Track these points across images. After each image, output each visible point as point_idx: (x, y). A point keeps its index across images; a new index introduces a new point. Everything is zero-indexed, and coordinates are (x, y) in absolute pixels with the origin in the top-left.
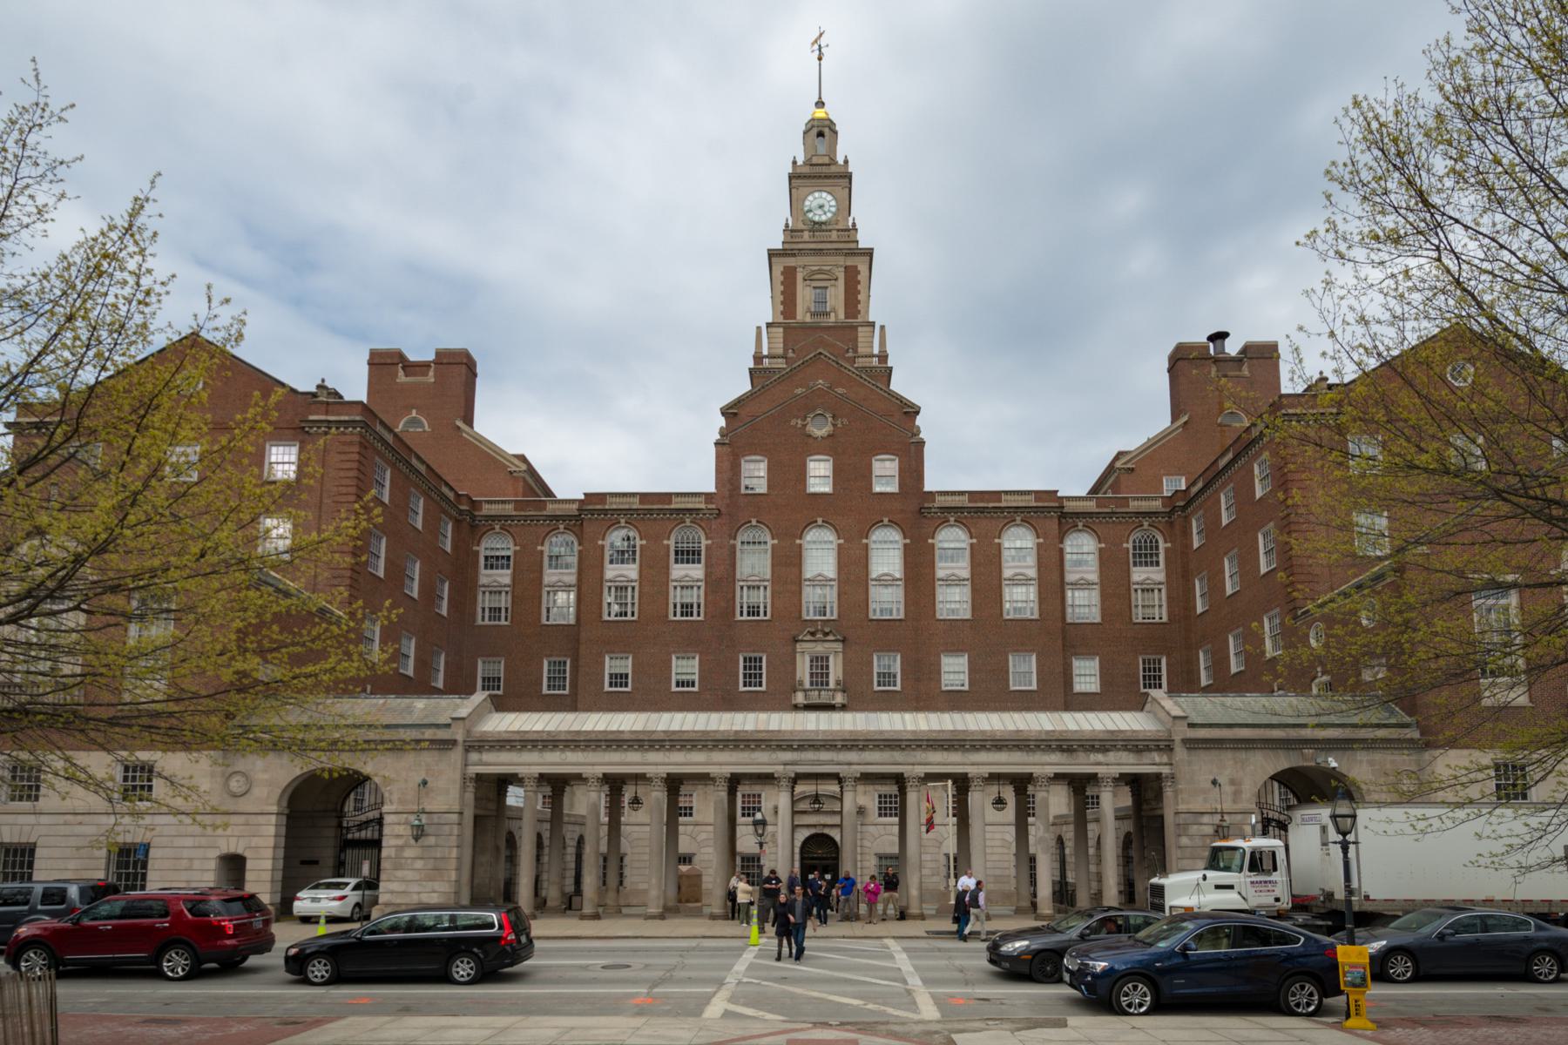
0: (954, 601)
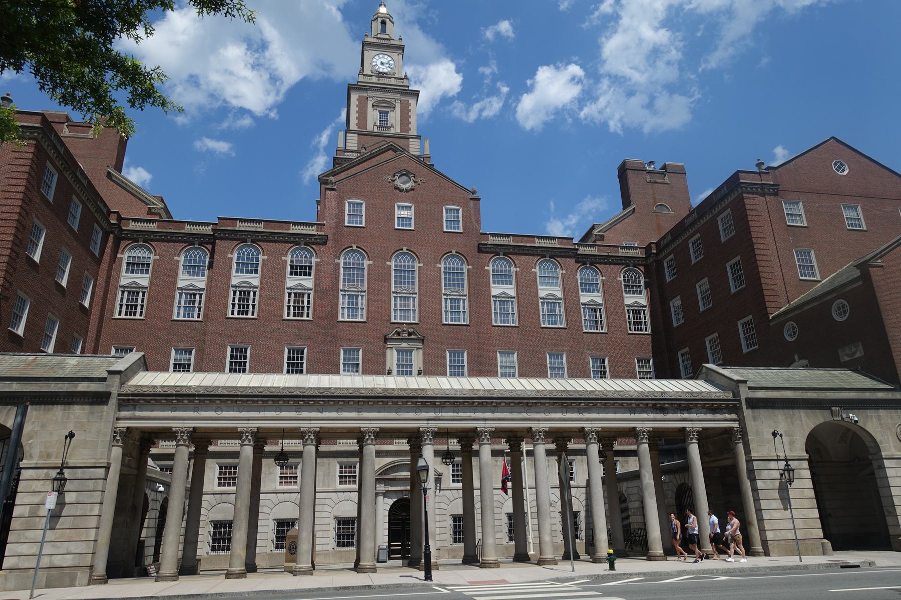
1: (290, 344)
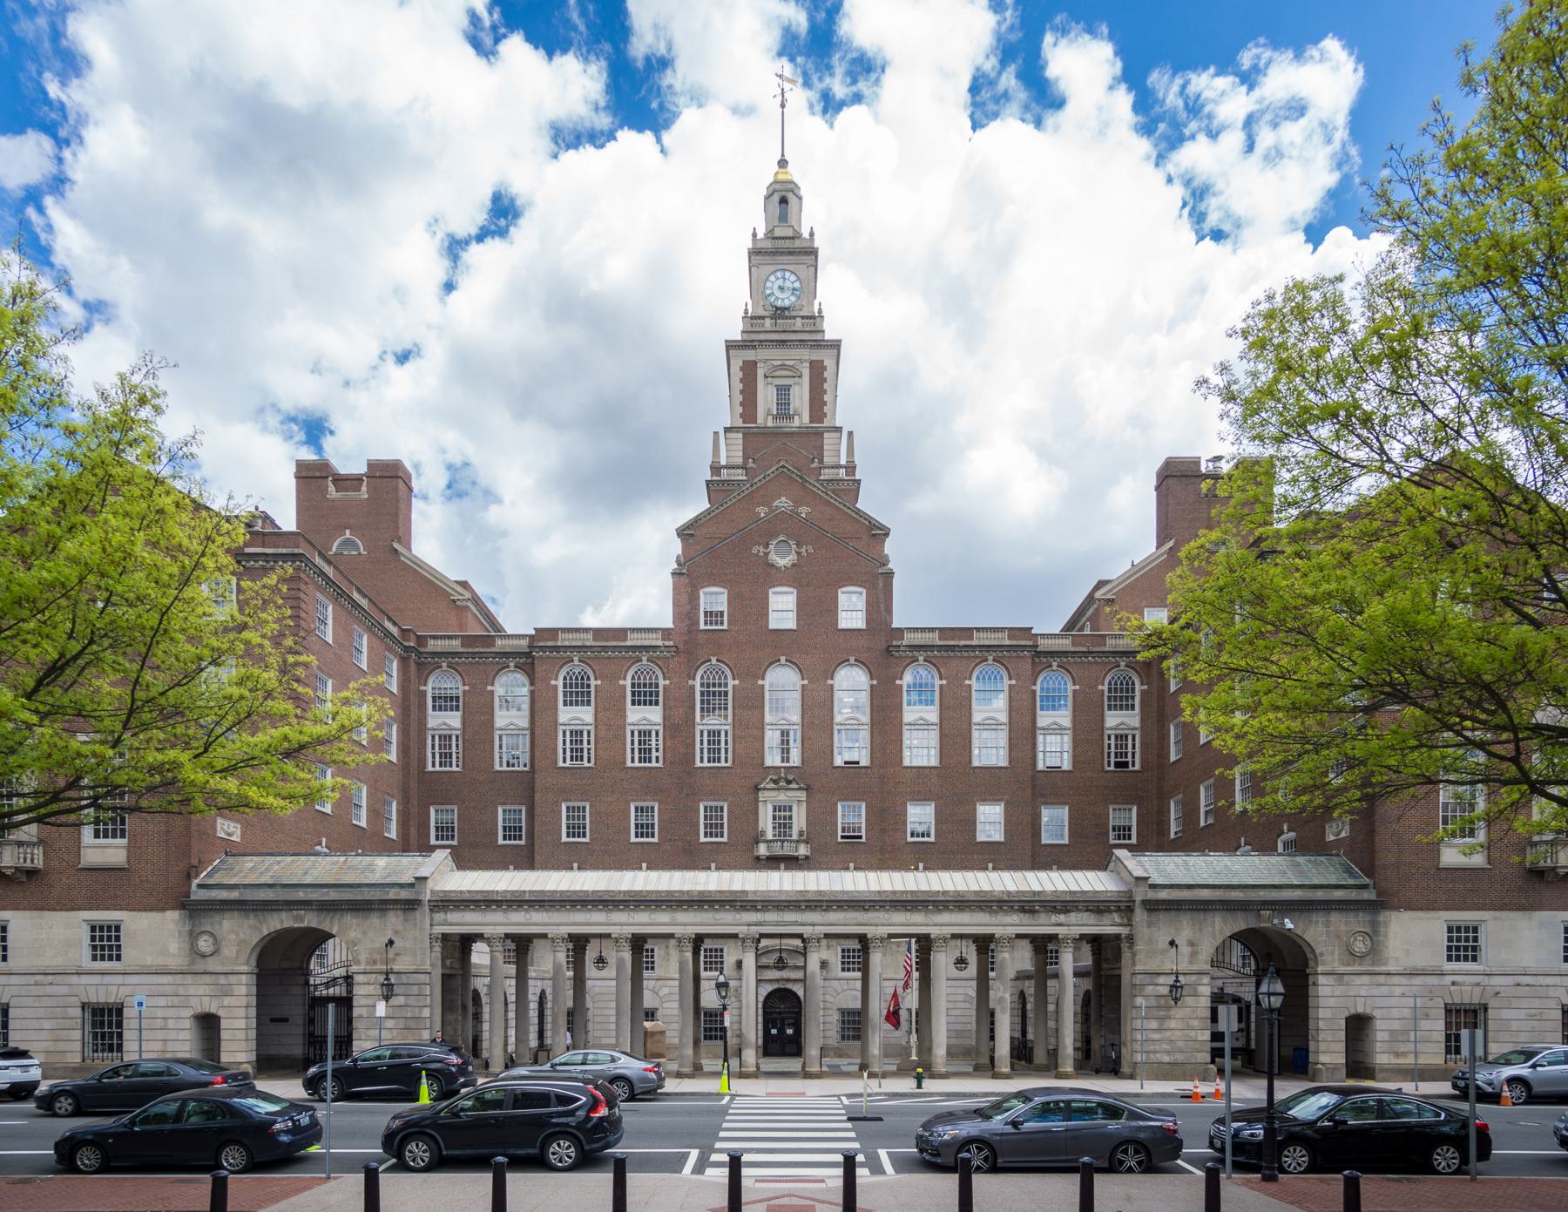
0: (920, 750)
1: (505, 804)
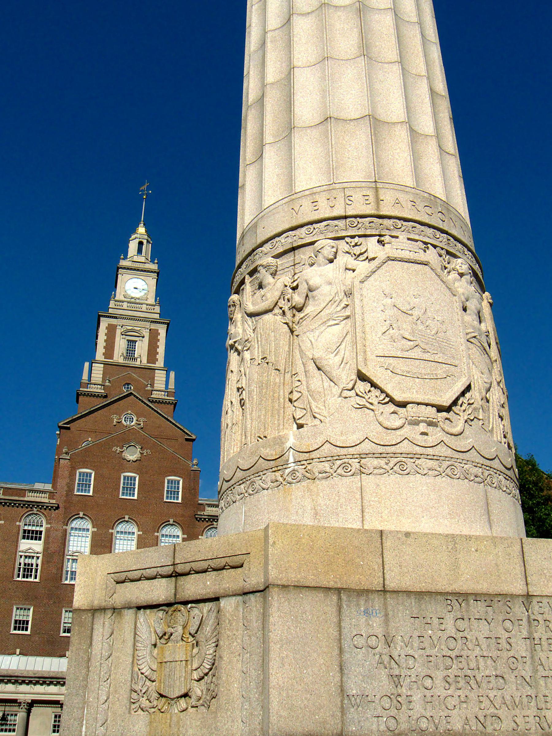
1: (19, 604)
